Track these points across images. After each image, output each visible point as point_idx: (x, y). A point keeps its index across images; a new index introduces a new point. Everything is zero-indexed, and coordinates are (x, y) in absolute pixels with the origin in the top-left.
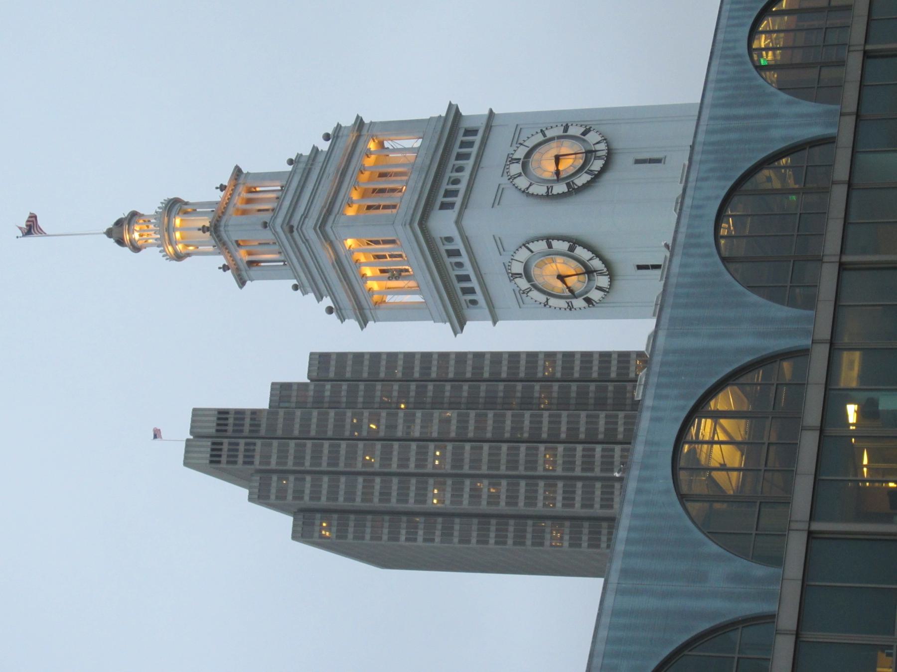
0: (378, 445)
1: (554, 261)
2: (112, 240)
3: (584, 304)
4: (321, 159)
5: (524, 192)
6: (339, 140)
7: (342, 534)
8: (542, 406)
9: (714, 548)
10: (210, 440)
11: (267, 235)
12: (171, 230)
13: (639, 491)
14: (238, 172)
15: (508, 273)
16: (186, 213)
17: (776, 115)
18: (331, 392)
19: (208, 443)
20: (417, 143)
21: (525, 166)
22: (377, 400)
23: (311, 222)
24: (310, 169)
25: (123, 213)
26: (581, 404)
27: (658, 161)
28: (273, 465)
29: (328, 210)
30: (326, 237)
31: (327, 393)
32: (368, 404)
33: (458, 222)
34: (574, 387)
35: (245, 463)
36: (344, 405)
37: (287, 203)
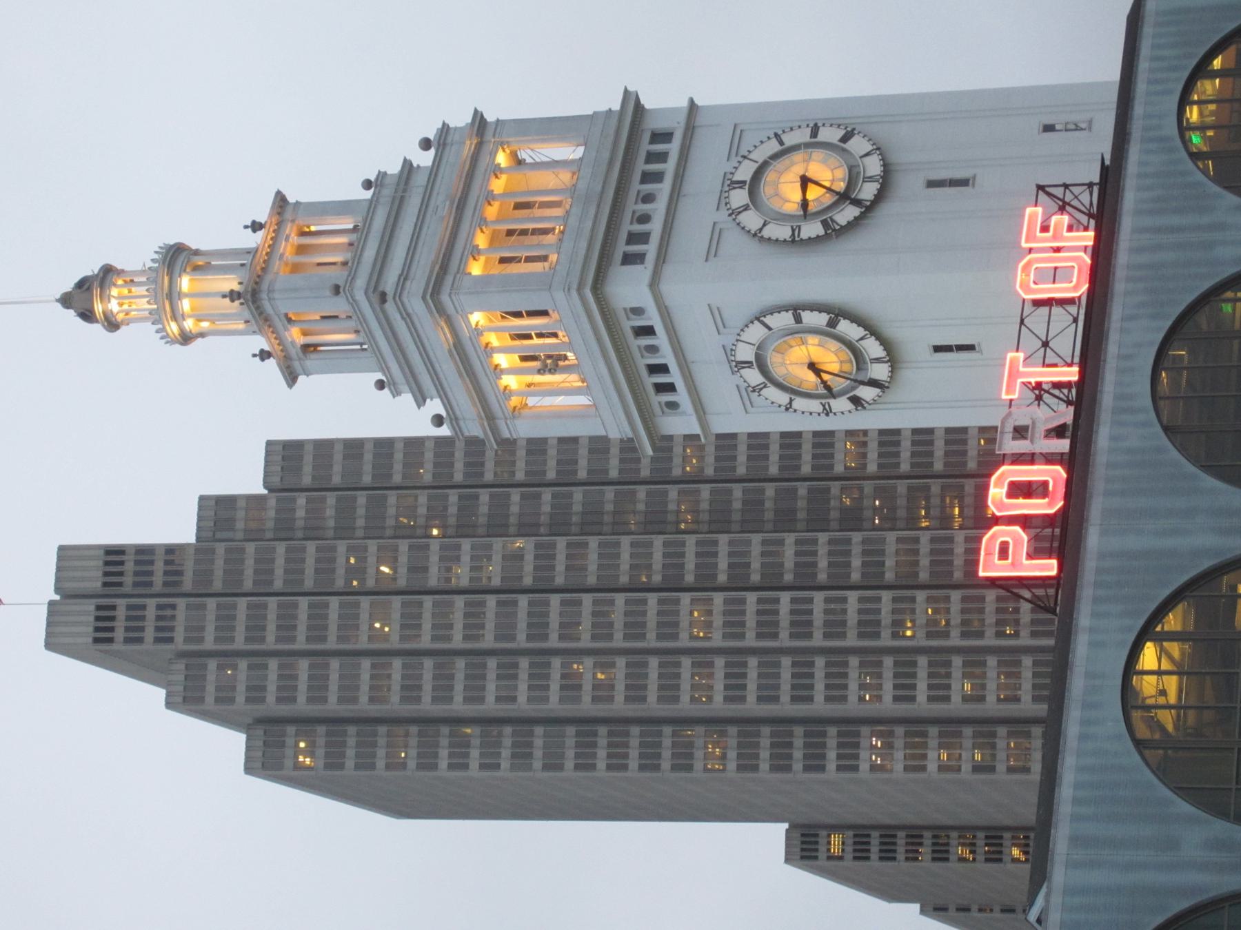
0: (397, 601)
1: (804, 342)
2: (72, 312)
3: (850, 406)
4: (420, 180)
5: (755, 235)
6: (448, 148)
7: (334, 761)
8: (683, 526)
9: (1185, 807)
10: (94, 601)
11: (339, 306)
12: (175, 295)
13: (1083, 737)
14: (281, 201)
15: (729, 362)
16: (196, 269)
17: (1221, 227)
18: (307, 511)
19: (90, 606)
20: (571, 152)
21: (752, 193)
22: (390, 522)
23: (417, 285)
24: (402, 199)
25: (91, 268)
26: (752, 523)
27: (964, 183)
28: (209, 644)
29: (441, 267)
30: (441, 310)
31: (300, 513)
32: (375, 530)
33: (654, 284)
34: (737, 491)
35: (158, 640)
36: (331, 533)
37: (370, 253)
